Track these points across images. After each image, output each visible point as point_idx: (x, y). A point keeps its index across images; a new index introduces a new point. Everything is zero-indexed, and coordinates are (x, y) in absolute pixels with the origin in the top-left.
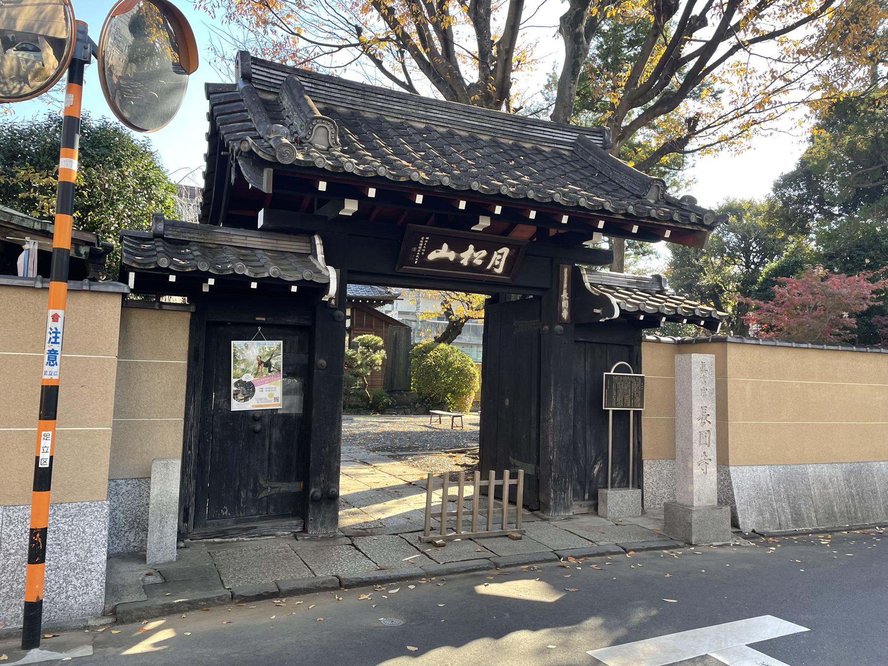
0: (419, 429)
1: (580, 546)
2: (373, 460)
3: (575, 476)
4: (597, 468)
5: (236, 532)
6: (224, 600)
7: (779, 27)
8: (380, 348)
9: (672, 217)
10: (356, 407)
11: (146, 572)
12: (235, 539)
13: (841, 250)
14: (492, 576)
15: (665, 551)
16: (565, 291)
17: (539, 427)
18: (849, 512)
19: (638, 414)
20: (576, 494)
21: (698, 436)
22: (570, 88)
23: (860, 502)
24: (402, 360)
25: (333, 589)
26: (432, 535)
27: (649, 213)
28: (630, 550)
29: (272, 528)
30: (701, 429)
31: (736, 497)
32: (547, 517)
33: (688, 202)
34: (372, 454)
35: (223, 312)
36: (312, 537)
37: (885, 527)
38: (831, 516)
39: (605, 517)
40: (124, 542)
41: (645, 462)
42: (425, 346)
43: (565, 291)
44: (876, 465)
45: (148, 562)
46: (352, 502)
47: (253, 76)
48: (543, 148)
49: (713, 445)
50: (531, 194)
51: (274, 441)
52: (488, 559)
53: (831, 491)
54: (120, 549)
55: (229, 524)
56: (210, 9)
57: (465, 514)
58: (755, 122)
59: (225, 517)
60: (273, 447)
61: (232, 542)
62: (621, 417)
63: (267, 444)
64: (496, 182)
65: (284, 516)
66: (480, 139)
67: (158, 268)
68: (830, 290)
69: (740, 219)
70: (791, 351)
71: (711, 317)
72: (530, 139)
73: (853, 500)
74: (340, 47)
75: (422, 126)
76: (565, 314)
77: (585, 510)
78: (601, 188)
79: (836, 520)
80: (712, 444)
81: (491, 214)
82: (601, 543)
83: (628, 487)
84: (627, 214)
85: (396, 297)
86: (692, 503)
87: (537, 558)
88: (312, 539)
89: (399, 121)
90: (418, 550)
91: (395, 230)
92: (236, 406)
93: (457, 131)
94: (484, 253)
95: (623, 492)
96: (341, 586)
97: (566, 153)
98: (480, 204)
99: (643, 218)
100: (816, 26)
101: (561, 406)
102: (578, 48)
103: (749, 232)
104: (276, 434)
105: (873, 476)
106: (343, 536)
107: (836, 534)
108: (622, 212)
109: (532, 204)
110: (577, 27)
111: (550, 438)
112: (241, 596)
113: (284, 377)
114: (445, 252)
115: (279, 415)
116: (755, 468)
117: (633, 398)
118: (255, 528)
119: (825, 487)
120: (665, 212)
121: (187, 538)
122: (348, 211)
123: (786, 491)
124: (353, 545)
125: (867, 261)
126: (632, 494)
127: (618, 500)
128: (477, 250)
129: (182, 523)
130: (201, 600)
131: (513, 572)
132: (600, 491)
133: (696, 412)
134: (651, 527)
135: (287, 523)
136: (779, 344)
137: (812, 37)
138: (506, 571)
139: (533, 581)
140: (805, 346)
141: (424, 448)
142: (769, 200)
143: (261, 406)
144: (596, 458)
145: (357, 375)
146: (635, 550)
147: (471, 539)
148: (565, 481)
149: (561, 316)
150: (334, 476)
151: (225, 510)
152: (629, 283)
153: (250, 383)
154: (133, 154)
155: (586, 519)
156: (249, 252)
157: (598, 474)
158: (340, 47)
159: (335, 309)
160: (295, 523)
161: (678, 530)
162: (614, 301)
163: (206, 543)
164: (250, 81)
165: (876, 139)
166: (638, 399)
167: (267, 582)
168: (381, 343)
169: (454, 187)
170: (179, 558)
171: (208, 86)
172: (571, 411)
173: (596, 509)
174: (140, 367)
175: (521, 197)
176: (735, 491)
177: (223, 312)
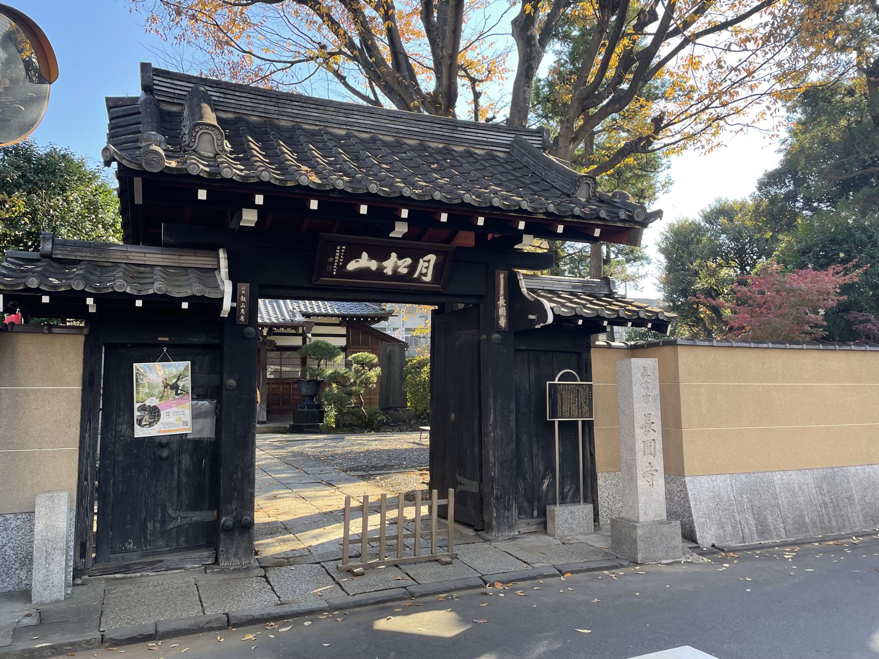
0: (405, 446)
1: (513, 569)
2: (340, 481)
3: (522, 492)
4: (546, 483)
5: (140, 566)
6: (92, 644)
7: (730, 15)
8: (375, 366)
9: (598, 214)
10: (351, 425)
11: (26, 613)
12: (138, 574)
13: (813, 245)
14: (400, 607)
15: (606, 572)
16: (501, 298)
17: (481, 442)
18: (822, 522)
19: (589, 426)
20: (521, 511)
21: (642, 446)
22: (524, 92)
23: (834, 510)
24: (396, 376)
25: (219, 629)
26: (351, 564)
27: (572, 211)
28: (566, 572)
29: (181, 560)
30: (645, 438)
31: (692, 510)
32: (488, 537)
33: (619, 199)
34: (343, 474)
35: (121, 331)
36: (222, 570)
37: (862, 536)
38: (801, 525)
39: (553, 536)
40: (15, 580)
41: (599, 475)
42: (419, 362)
43: (501, 298)
44: (852, 470)
45: (34, 602)
46: (275, 529)
47: (155, 87)
48: (477, 151)
49: (660, 455)
50: (438, 196)
51: (183, 468)
52: (405, 588)
53: (801, 499)
54: (10, 588)
55: (135, 558)
56: (161, 32)
57: (388, 538)
58: (718, 118)
59: (130, 551)
60: (182, 474)
61: (136, 577)
62: (568, 428)
63: (176, 471)
64: (516, 198)
65: (196, 547)
66: (476, 154)
67: (28, 289)
68: (788, 286)
69: (731, 220)
70: (750, 352)
71: (658, 319)
72: (461, 141)
73: (826, 508)
74: (293, 63)
75: (343, 132)
76: (503, 322)
77: (533, 528)
78: (530, 188)
79: (807, 531)
80: (658, 454)
81: (252, 205)
82: (537, 565)
83: (579, 502)
84: (547, 213)
85: (390, 314)
86: (638, 518)
87: (458, 585)
88: (222, 571)
89: (317, 128)
90: (334, 580)
91: (305, 237)
92: (140, 432)
93: (381, 137)
94: (408, 261)
95: (573, 508)
96: (229, 625)
97: (501, 155)
98: (385, 209)
99: (567, 217)
100: (770, 13)
101: (508, 417)
102: (531, 51)
103: (740, 233)
104: (186, 460)
105: (849, 482)
106: (257, 567)
107: (806, 546)
108: (542, 211)
109: (442, 206)
110: (528, 29)
111: (491, 453)
112: (111, 639)
113: (193, 399)
114: (365, 262)
115: (189, 440)
116: (714, 477)
117: (580, 407)
118: (161, 561)
119: (794, 495)
120: (591, 209)
121: (85, 574)
122: (399, 232)
123: (750, 501)
124: (265, 577)
125: (842, 255)
126: (584, 510)
127: (569, 517)
128: (400, 258)
129: (78, 559)
130: (65, 645)
131: (428, 602)
132: (549, 508)
133: (639, 420)
134: (598, 545)
135: (197, 554)
136: (735, 344)
137: (766, 24)
138: (415, 600)
139: (443, 612)
140: (765, 345)
141: (400, 466)
142: (754, 198)
143: (164, 432)
144: (545, 472)
145: (350, 394)
146: (572, 572)
147: (396, 566)
148: (509, 498)
149: (498, 324)
150: (248, 504)
151: (129, 543)
152: (574, 287)
153: (155, 408)
154: (79, 179)
155: (532, 538)
156: (148, 269)
157: (547, 490)
158: (293, 63)
159: (246, 326)
160: (206, 554)
161: (624, 547)
162: (547, 305)
163: (107, 580)
164: (152, 93)
165: (848, 127)
166: (586, 409)
167: (146, 623)
168: (376, 360)
169: (349, 190)
170: (68, 597)
171: (108, 99)
172: (513, 424)
173: (545, 528)
174: (29, 395)
175: (427, 198)
176: (692, 503)
177: (121, 331)
